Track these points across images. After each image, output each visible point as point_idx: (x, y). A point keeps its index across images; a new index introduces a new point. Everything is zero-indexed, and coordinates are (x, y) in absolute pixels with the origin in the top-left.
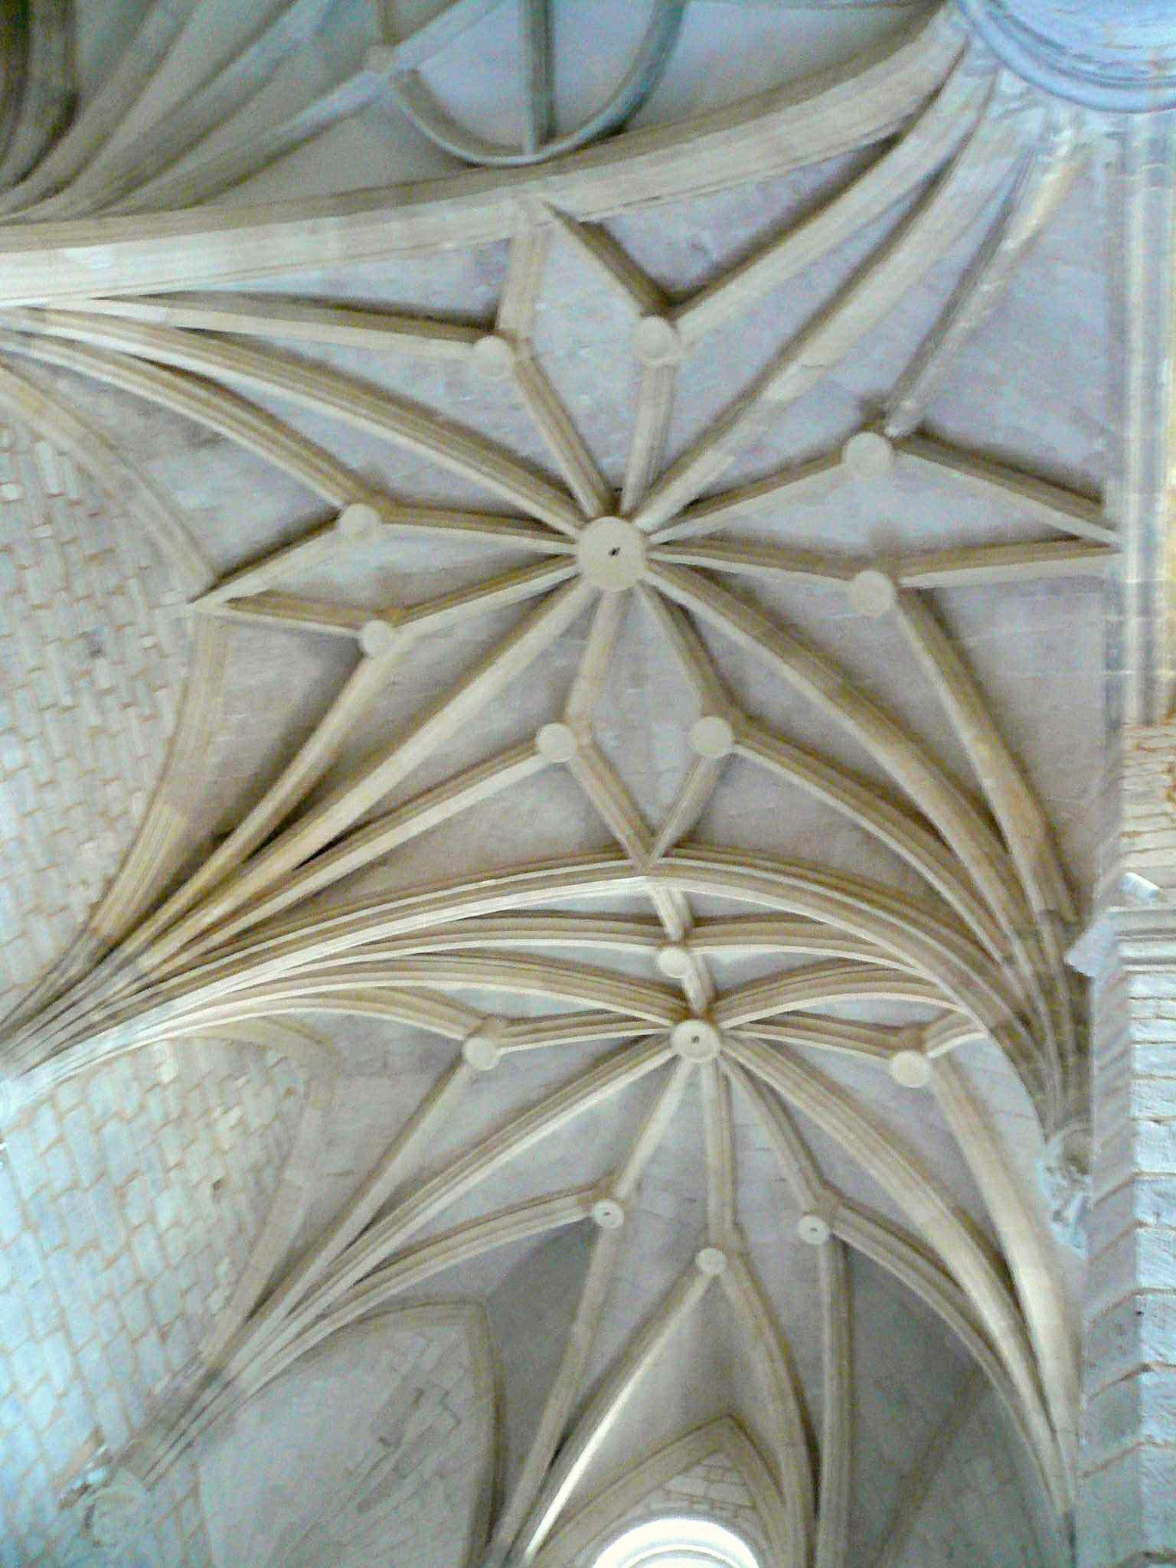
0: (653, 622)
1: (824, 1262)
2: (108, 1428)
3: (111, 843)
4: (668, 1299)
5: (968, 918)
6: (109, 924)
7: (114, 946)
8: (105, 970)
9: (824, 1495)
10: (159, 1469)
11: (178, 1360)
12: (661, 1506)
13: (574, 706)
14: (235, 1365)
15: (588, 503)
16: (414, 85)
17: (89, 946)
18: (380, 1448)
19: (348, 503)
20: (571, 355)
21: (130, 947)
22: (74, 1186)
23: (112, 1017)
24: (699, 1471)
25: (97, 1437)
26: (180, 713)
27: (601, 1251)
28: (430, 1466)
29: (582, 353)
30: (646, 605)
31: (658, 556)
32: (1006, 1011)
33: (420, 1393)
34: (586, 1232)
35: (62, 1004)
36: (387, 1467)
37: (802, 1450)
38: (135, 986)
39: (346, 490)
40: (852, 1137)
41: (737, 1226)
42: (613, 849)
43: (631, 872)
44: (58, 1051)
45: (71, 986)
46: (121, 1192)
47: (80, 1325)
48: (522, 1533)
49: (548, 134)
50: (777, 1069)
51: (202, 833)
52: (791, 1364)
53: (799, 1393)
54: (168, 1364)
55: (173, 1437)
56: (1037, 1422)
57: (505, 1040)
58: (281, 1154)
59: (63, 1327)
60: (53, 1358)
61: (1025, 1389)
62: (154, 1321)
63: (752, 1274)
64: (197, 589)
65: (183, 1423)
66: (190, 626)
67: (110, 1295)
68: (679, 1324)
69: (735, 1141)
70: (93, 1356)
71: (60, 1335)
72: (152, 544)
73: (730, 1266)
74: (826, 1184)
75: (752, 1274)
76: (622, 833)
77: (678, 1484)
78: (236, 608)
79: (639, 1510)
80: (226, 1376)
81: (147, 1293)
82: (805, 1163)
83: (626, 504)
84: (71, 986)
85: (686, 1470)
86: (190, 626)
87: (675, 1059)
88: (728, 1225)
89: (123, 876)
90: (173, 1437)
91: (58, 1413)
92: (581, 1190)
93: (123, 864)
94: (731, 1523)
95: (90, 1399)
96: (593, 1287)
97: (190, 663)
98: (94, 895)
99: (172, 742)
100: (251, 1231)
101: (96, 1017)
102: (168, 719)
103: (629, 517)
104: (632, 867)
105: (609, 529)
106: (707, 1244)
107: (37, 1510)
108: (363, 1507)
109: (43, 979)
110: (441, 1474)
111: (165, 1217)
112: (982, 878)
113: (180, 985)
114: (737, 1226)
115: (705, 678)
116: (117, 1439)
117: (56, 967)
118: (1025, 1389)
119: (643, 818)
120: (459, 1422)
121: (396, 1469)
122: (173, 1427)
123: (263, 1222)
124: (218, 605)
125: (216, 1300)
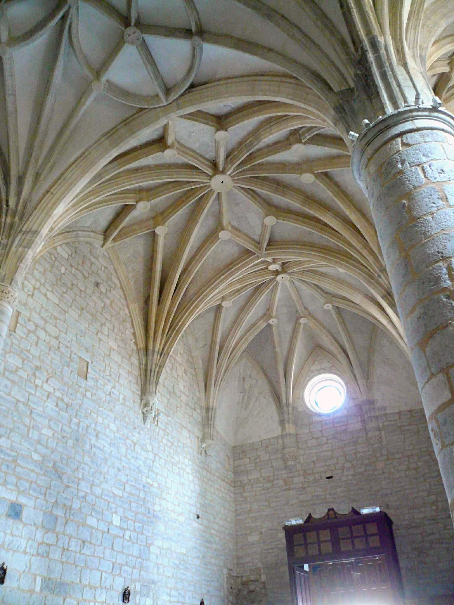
0: (242, 196)
1: (333, 312)
2: (198, 435)
3: (129, 325)
4: (295, 331)
5: (363, 262)
6: (142, 345)
7: (147, 349)
8: (150, 357)
9: (352, 362)
10: (212, 434)
11: (199, 411)
12: (312, 375)
13: (225, 223)
14: (211, 404)
15: (210, 172)
16: (112, 87)
17: (142, 353)
18: (242, 394)
19: (137, 202)
20: (189, 136)
21: (151, 347)
22: (168, 400)
23: (160, 366)
24: (316, 363)
25: (198, 438)
26: (118, 278)
27: (274, 329)
28: (256, 393)
29: (192, 135)
30: (236, 191)
31: (234, 178)
32: (385, 293)
33: (244, 378)
34: (269, 326)
35: (149, 371)
36: (246, 397)
37: (343, 354)
38: (159, 356)
39: (134, 198)
40: (333, 287)
41: (305, 308)
42: (248, 252)
43: (258, 257)
44: (157, 383)
45: (146, 365)
46: (174, 393)
47: (184, 423)
48: (287, 399)
49: (168, 91)
50: (307, 276)
51: (142, 303)
52: (331, 334)
53: (336, 340)
54: (198, 414)
55: (210, 426)
56: (402, 343)
57: (231, 298)
58: (190, 351)
59: (183, 426)
60: (185, 433)
61: (396, 336)
62: (192, 409)
63: (315, 319)
64: (102, 243)
65: (210, 423)
66: (106, 254)
67: (185, 412)
68: (300, 336)
69: (297, 290)
70: (189, 425)
71: (184, 429)
72: (87, 243)
73: (308, 319)
74: (326, 293)
75: (315, 319)
76: (251, 248)
77: (313, 368)
78: (115, 242)
79: (308, 378)
80: (211, 407)
81: (188, 405)
82: (319, 290)
83: (221, 168)
84: (146, 365)
85: (314, 363)
86: (106, 254)
87: (70, 7)
88: (303, 309)
89: (136, 330)
90: (210, 426)
91: (191, 441)
92: (262, 317)
93: (133, 327)
94: (330, 372)
95: (193, 433)
96: (276, 338)
97: (112, 263)
98: (134, 340)
99: (122, 287)
100: (194, 373)
101: (157, 370)
102: (117, 281)
103: (223, 172)
104: (258, 256)
105: (219, 178)
106: (301, 318)
107: (198, 459)
108: (245, 409)
109: (140, 368)
110: (259, 393)
111: (182, 388)
112: (365, 253)
113: (168, 349)
114: (305, 308)
115: (260, 203)
116: (200, 435)
117: (140, 364)
118: (396, 336)
119: (254, 240)
120: (257, 381)
121: (248, 397)
122: (208, 425)
123: (195, 369)
124: (111, 243)
125: (198, 394)
